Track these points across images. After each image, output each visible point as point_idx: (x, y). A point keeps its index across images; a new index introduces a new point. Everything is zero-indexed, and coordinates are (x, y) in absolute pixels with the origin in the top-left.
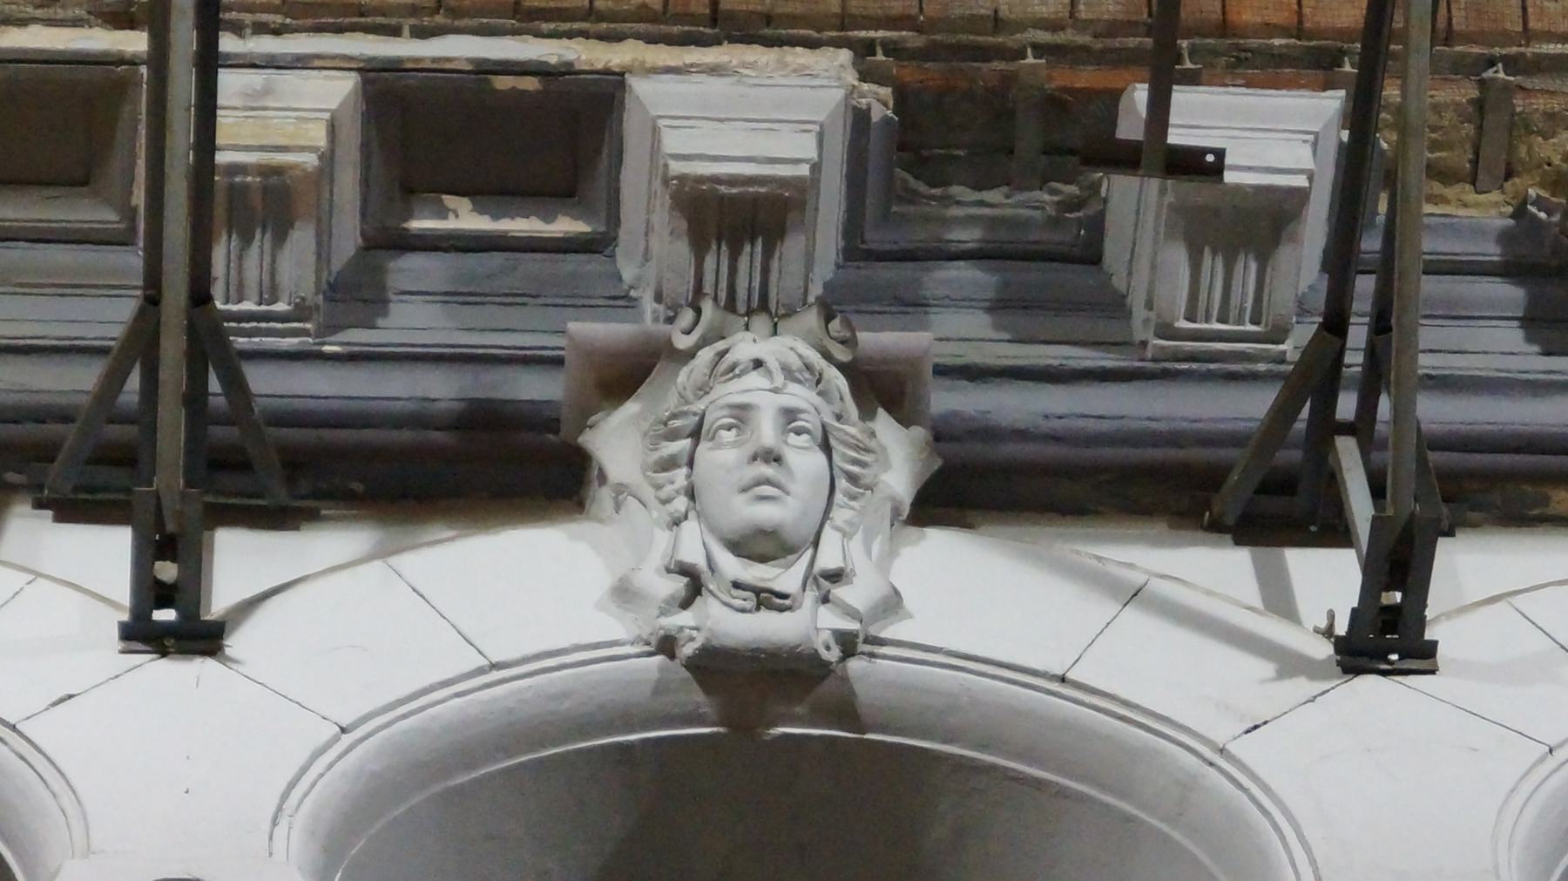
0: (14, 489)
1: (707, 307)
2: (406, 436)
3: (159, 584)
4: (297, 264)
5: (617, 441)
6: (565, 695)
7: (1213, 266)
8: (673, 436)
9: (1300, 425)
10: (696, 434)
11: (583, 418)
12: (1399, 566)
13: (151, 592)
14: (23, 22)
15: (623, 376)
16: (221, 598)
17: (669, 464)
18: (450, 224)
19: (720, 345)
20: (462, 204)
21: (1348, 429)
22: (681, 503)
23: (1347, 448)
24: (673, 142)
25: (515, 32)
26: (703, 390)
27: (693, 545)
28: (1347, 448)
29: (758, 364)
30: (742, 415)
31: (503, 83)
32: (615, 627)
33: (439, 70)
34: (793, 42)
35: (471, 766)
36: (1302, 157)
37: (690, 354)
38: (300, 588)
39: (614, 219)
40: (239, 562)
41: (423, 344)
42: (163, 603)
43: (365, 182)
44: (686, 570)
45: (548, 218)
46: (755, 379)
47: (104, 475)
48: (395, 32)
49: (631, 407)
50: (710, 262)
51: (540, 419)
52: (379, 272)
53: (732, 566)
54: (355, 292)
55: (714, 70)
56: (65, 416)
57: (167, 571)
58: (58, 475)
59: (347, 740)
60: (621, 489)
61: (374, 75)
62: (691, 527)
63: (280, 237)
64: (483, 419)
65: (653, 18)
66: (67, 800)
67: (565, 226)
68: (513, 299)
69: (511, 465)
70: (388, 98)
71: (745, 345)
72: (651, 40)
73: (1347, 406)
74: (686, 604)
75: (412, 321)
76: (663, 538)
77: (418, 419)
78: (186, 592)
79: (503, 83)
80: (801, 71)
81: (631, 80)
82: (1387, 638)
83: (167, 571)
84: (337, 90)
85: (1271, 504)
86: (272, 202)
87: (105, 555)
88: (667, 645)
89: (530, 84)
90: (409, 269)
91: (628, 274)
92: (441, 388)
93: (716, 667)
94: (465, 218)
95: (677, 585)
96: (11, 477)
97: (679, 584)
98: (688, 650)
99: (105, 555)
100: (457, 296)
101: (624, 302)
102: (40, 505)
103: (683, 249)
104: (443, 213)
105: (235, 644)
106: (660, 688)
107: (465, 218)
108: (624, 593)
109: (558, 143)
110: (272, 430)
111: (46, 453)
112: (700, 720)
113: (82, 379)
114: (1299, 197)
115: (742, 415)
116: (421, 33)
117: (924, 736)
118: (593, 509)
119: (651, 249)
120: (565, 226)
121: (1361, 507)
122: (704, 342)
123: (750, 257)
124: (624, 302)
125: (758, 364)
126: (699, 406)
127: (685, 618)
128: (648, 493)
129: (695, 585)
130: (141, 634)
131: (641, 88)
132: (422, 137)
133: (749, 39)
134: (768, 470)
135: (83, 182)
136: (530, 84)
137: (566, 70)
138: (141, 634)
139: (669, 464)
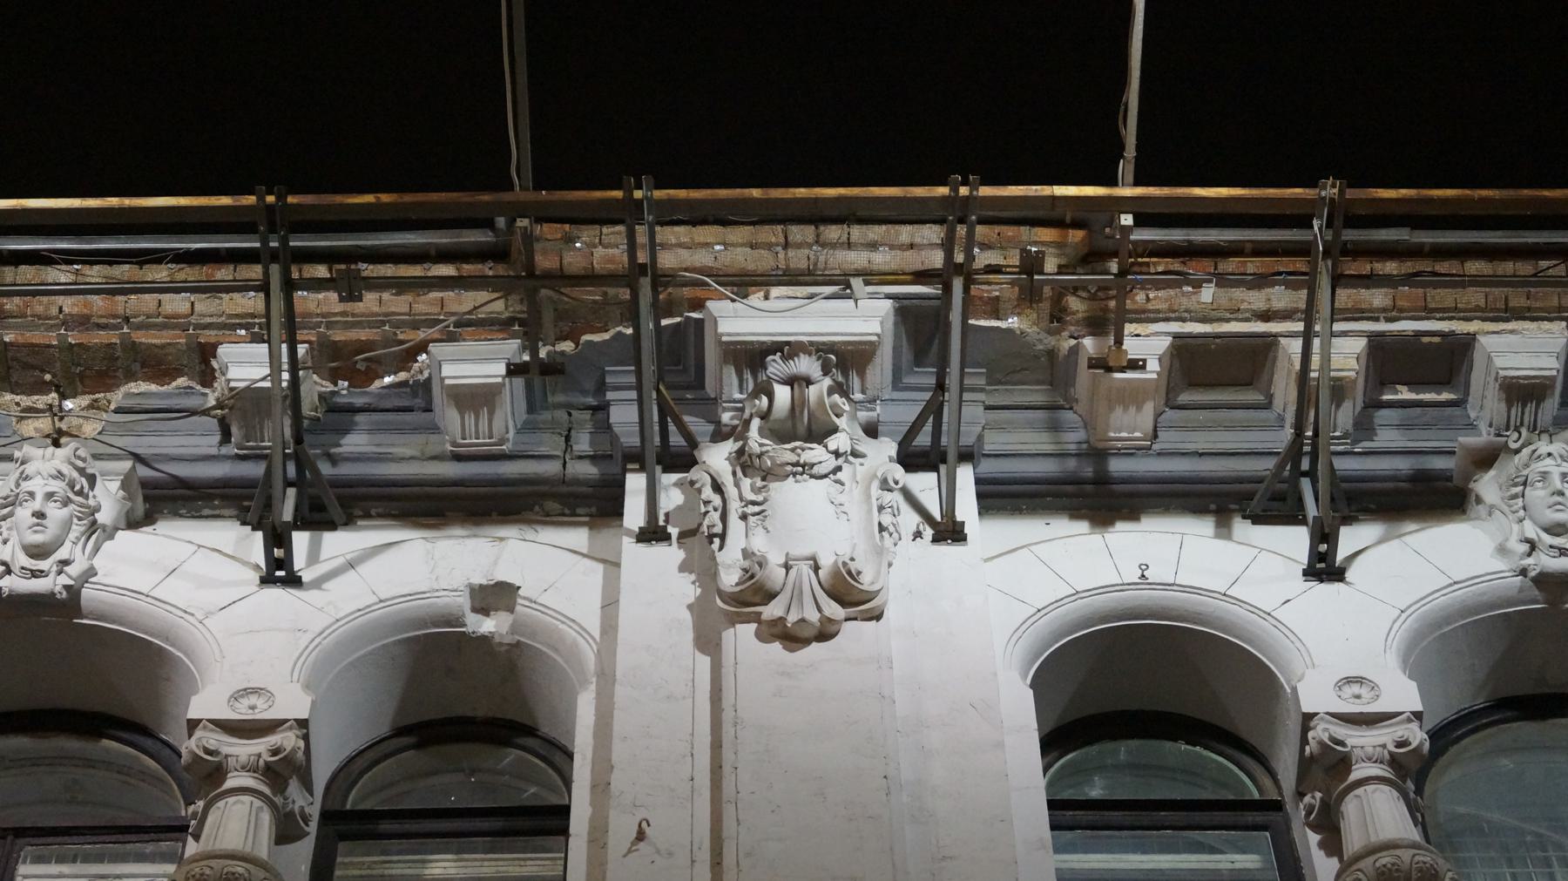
0: (1234, 511)
1: (1524, 431)
2: (1391, 485)
3: (277, 560)
4: (1345, 417)
5: (1488, 486)
6: (1484, 594)
7: (470, 420)
8: (1516, 485)
9: (1286, 473)
10: (1525, 484)
11: (1468, 478)
12: (1324, 536)
13: (275, 564)
14: (1228, 320)
15: (1486, 459)
16: (1342, 553)
17: (1515, 497)
18: (1399, 397)
19: (1532, 447)
20: (1403, 389)
21: (1305, 474)
22: (1522, 513)
23: (1306, 484)
24: (1499, 362)
25: (1428, 319)
26: (1527, 466)
27: (1531, 531)
28: (1306, 484)
29: (1550, 455)
30: (1544, 476)
31: (1426, 340)
32: (1499, 565)
33: (1400, 335)
34: (1543, 319)
35: (1449, 624)
36: (1353, 364)
37: (1517, 451)
38: (1369, 552)
39: (1467, 393)
40: (1350, 539)
41: (1391, 448)
42: (280, 569)
43: (1366, 381)
44: (1528, 541)
45: (1439, 393)
46: (1549, 461)
47: (1275, 504)
48: (1377, 319)
49: (1492, 473)
50: (1527, 410)
51: (1445, 476)
52: (1371, 417)
53: (1548, 539)
54: (1364, 427)
55: (1512, 332)
56: (1260, 481)
57: (278, 553)
58: (1255, 505)
59: (1404, 616)
60: (1492, 507)
61: (1373, 337)
62: (1527, 523)
63: (1139, 409)
64: (1422, 478)
65: (1482, 310)
66: (1298, 644)
67: (1445, 396)
68: (1427, 426)
69: (1434, 496)
70: (1377, 344)
71: (1543, 447)
72: (1484, 320)
73: (1305, 465)
74: (1529, 555)
75: (1387, 437)
76: (1516, 527)
77: (1394, 478)
78: (285, 563)
79: (1426, 340)
80: (1547, 331)
81: (1282, 340)
82: (1324, 568)
83: (1323, 548)
84: (1360, 344)
85: (1276, 507)
86: (1339, 390)
87: (1295, 541)
88: (1523, 572)
89: (1437, 340)
90: (1383, 415)
91: (1473, 415)
92: (1403, 465)
93: (1544, 581)
94: (1405, 394)
95: (1525, 547)
96: (1233, 506)
97: (1526, 547)
98: (1533, 574)
99: (1295, 541)
100: (1404, 426)
101: (1471, 427)
102: (1244, 517)
103: (1503, 406)
104: (1396, 392)
105: (1349, 575)
106: (1521, 590)
107: (1405, 394)
108: (1502, 550)
109: (1447, 363)
110: (1344, 485)
111: (1250, 496)
112: (1537, 602)
113: (1266, 465)
114: (1553, 379)
115: (1544, 476)
116: (1389, 320)
117: (113, 622)
118: (1473, 515)
119: (1486, 406)
120: (1445, 396)
121: (1312, 511)
122: (1523, 446)
123: (1530, 408)
124: (1471, 427)
125: (1550, 455)
126: (1525, 472)
127: (1530, 561)
128: (1506, 509)
129: (1533, 546)
130: (1312, 573)
131: (1482, 339)
132: (1389, 361)
133: (1524, 319)
134: (1559, 499)
135: (1250, 384)
136: (1437, 340)
137: (1452, 333)
138: (1312, 573)
139: (1515, 497)
